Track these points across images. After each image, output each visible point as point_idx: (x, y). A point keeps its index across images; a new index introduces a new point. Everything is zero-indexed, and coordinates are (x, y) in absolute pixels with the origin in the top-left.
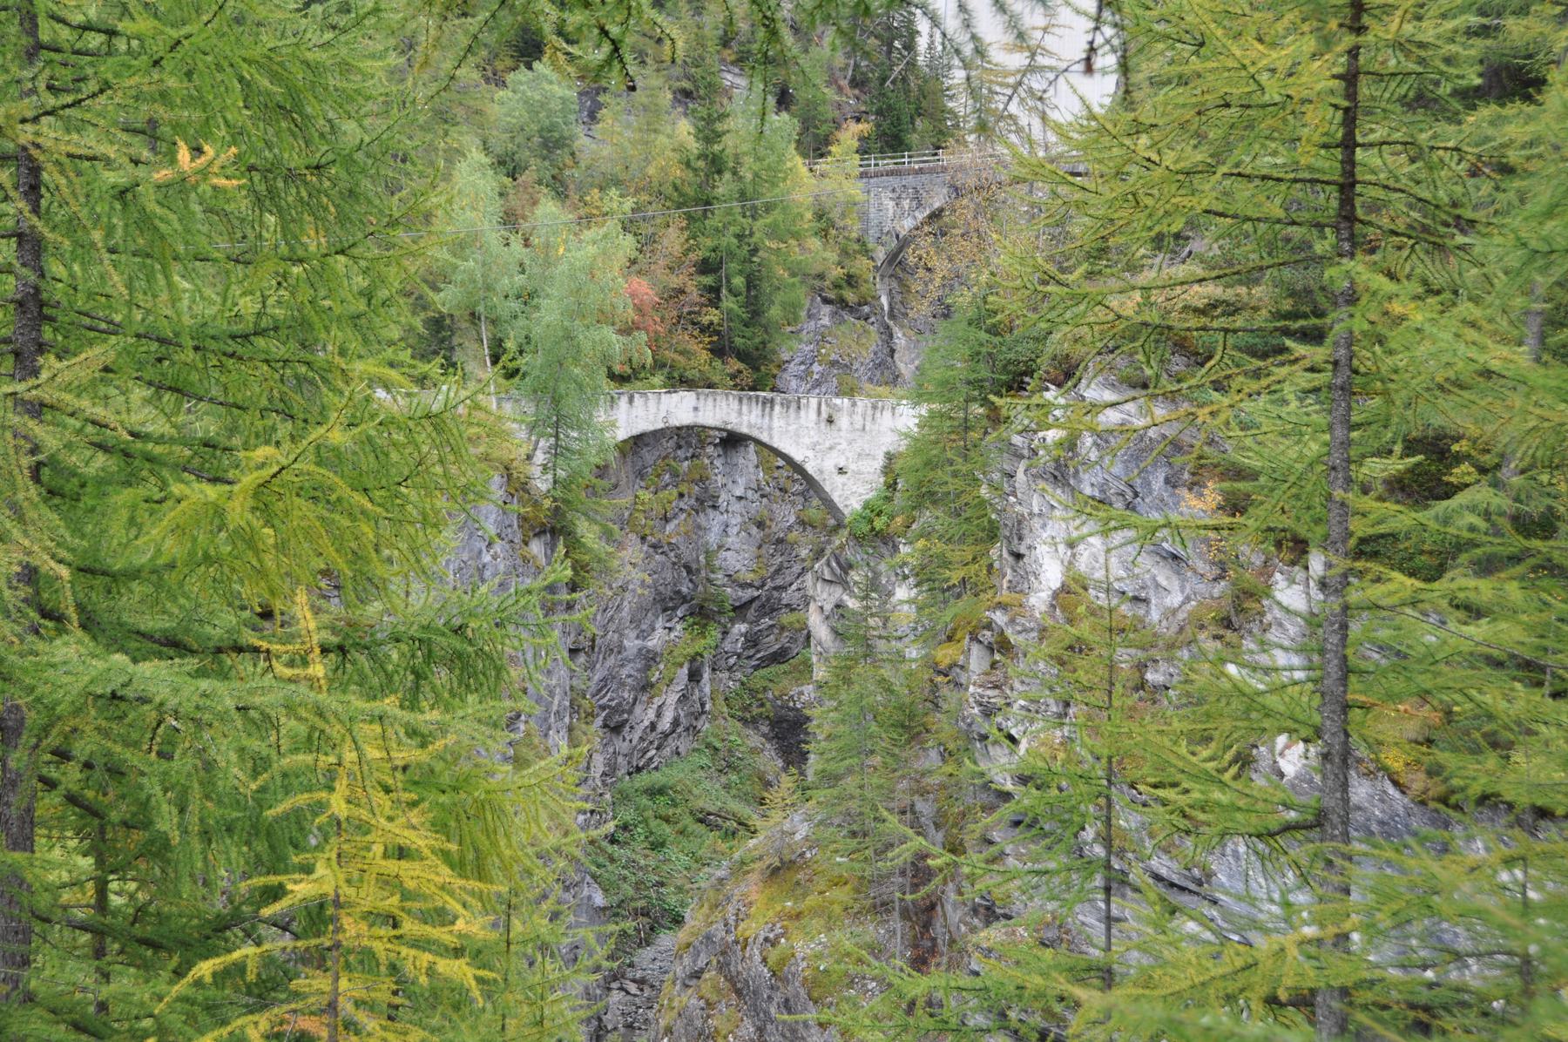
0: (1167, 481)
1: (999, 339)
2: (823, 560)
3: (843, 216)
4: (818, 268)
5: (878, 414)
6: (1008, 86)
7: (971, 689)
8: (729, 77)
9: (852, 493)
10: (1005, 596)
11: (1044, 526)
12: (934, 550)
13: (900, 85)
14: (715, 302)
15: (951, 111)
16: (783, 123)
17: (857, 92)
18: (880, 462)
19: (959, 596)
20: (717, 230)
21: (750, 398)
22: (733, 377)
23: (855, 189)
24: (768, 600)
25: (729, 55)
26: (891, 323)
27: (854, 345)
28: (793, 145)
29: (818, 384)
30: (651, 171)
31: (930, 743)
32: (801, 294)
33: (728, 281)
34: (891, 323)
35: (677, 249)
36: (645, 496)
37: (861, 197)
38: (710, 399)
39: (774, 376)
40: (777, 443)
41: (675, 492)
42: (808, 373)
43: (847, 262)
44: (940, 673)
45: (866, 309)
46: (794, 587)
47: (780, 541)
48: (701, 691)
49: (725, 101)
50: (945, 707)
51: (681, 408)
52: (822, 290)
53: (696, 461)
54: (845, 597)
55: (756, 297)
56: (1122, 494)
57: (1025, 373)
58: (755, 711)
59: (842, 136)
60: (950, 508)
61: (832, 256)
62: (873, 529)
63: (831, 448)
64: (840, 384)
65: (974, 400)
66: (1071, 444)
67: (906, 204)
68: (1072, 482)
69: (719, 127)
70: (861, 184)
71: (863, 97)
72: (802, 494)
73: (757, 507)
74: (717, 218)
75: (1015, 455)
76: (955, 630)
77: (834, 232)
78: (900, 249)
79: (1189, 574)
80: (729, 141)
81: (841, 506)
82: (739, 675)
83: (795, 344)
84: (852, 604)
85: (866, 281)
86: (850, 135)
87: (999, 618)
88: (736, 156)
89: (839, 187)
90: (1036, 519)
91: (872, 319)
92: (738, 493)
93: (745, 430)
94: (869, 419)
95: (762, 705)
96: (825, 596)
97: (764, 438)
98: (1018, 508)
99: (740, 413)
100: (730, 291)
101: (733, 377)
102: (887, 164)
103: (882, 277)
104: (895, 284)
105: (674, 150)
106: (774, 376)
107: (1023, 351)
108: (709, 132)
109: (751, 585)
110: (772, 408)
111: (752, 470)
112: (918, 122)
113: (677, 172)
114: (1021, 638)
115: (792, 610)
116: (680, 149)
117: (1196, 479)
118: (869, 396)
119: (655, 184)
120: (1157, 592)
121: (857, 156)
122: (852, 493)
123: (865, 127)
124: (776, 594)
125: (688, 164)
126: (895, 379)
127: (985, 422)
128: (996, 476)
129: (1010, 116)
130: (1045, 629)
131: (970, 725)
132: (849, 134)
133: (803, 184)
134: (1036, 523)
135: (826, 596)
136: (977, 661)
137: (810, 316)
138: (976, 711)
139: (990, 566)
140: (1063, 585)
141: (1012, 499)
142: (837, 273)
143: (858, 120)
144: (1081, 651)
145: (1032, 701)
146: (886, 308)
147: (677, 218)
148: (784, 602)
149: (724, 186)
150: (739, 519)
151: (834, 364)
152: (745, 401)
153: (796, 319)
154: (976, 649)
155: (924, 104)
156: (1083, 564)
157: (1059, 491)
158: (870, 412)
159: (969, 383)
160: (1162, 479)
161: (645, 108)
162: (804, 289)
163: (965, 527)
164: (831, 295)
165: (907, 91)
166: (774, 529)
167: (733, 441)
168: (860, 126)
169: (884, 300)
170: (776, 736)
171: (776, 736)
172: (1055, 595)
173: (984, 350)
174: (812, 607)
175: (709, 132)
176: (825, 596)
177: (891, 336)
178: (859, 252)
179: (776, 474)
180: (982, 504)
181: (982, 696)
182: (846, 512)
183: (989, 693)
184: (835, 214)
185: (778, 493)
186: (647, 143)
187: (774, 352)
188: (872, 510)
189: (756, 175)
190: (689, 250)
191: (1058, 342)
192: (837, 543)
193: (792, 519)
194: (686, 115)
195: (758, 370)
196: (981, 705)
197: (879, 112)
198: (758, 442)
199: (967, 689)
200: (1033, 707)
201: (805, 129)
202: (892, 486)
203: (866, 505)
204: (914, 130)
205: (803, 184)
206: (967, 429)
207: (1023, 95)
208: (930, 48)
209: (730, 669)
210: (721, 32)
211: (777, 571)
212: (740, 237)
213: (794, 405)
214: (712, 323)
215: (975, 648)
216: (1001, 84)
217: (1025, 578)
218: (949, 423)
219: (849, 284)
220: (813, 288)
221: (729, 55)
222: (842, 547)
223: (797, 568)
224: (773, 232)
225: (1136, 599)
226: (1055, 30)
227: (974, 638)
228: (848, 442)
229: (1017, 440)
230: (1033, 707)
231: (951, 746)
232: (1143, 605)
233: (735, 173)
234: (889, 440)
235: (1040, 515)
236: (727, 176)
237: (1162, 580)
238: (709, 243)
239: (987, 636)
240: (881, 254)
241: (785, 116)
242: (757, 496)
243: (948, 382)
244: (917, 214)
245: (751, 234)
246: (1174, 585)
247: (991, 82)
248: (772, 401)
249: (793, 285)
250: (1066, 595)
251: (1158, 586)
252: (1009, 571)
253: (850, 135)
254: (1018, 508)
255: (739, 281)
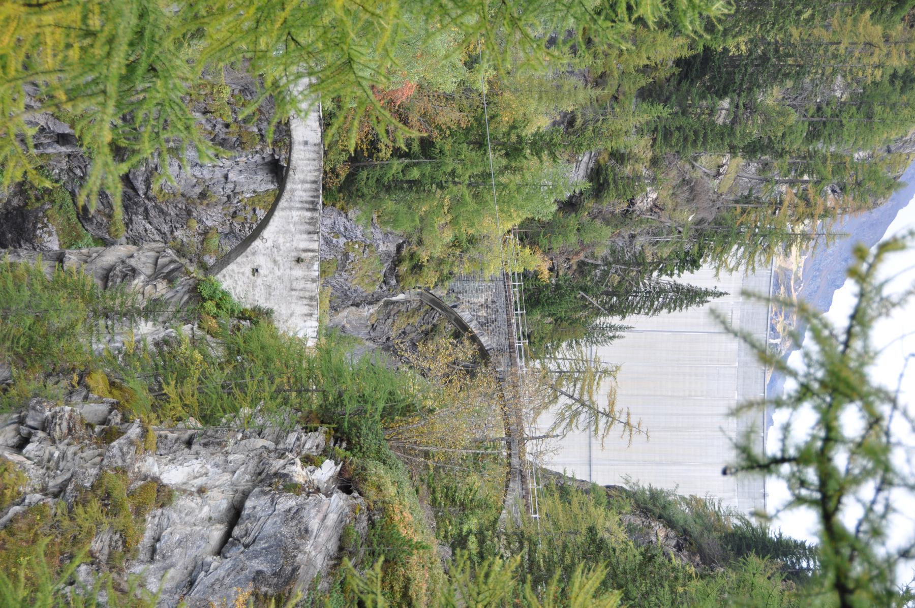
0: (259, 573)
1: (377, 417)
2: (175, 257)
3: (472, 260)
4: (427, 241)
5: (305, 302)
6: (581, 394)
7: (68, 408)
8: (586, 159)
9: (236, 281)
10: (153, 436)
11: (217, 465)
12: (193, 368)
13: (581, 303)
14: (397, 153)
15: (558, 345)
16: (549, 210)
17: (575, 267)
18: (264, 304)
19: (151, 390)
20: (458, 154)
21: (317, 190)
22: (333, 170)
23: (493, 270)
24: (136, 203)
25: (604, 158)
26: (381, 303)
27: (362, 272)
28: (530, 216)
29: (328, 242)
30: (507, 95)
31: (14, 370)
32: (407, 227)
33: (415, 165)
34: (381, 303)
35: (441, 120)
36: (226, 95)
37: (487, 274)
38: (315, 156)
39: (334, 205)
40: (278, 214)
41: (230, 120)
42: (337, 234)
43: (433, 264)
44: (81, 377)
45: (393, 282)
46: (148, 226)
47: (189, 213)
48: (49, 145)
49: (566, 157)
50: (50, 383)
51: (306, 131)
52: (409, 244)
53: (258, 138)
54: (142, 277)
55: (402, 188)
56: (247, 534)
57: (349, 443)
58: (32, 194)
59: (539, 256)
60: (228, 376)
61: (438, 252)
62: (204, 300)
63: (275, 262)
64: (329, 262)
65: (326, 399)
66: (293, 488)
67: (483, 313)
68: (257, 489)
69: (545, 154)
70: (498, 274)
71: (570, 272)
72: (232, 231)
73: (219, 192)
74: (468, 154)
75: (278, 436)
76: (120, 388)
77: (458, 253)
78: (444, 309)
79: (177, 597)
80: (534, 162)
81: (224, 271)
82: (65, 178)
83: (363, 221)
84: (138, 282)
85: (417, 281)
86: (539, 263)
87: (134, 431)
88: (521, 169)
89: (495, 262)
90: (223, 458)
91: (384, 288)
92: (231, 176)
93: (289, 186)
94: (302, 294)
95: (38, 199)
96: (143, 259)
97: (283, 203)
98: (232, 441)
99: (304, 182)
100: (407, 166)
101: (333, 170)
102: (515, 295)
103: (421, 294)
104: (415, 305)
105: (525, 114)
106: (334, 205)
107: (369, 441)
108: (542, 145)
109: (148, 188)
110: (308, 210)
111: (252, 187)
112: (550, 319)
113: (506, 118)
114: (115, 451)
115: (127, 225)
116: (526, 120)
117: (261, 598)
118: (321, 293)
119: (496, 99)
120: (159, 569)
121: (522, 271)
122: (236, 281)
123: (545, 275)
124: (141, 210)
125: (513, 127)
126: (335, 309)
127: (306, 408)
128: (259, 421)
129: (556, 398)
130: (124, 472)
131: (34, 408)
132: (540, 262)
133: (497, 225)
134: (219, 458)
135: (143, 260)
136: (93, 410)
137: (386, 235)
138: (48, 413)
139: (179, 419)
140: (164, 486)
141: (240, 436)
142: (424, 256)
143: (551, 270)
144: (106, 505)
145: (58, 463)
146: (394, 299)
147: (466, 120)
148: (134, 218)
149: (494, 159)
150: (207, 177)
151: (346, 255)
152: (314, 186)
153: (385, 223)
154: (103, 408)
155: (565, 324)
156: (184, 502)
157: (248, 477)
158: (307, 294)
159: (340, 395)
160: (260, 568)
161: (559, 87)
162: (410, 230)
163: (215, 397)
164: (405, 252)
165: (575, 310)
166: (200, 208)
167: (278, 171)
168: (546, 272)
169: (401, 297)
170: (8, 212)
171: (8, 212)
172: (156, 480)
173: (369, 406)
174: (132, 248)
175: (542, 145)
176: (143, 259)
177: (370, 303)
178: (441, 275)
179: (249, 208)
180: (236, 410)
181: (61, 418)
182: (219, 276)
183: (65, 424)
184: (473, 253)
185: (232, 210)
186: (530, 91)
187: (355, 204)
188: (221, 300)
189: (505, 186)
190: (441, 130)
191: (376, 470)
192: (191, 269)
193: (209, 223)
194: (554, 124)
195: (340, 191)
196: (53, 417)
197: (558, 287)
198: (278, 199)
199: (67, 403)
200: (52, 464)
201: (543, 225)
202: (243, 316)
203: (225, 294)
204: (544, 317)
205: (497, 225)
206: (299, 392)
207: (574, 408)
208: (611, 327)
209: (70, 170)
210: (622, 151)
211: (162, 211)
212: (453, 173)
213: (311, 228)
214: (379, 151)
215: (104, 408)
216: (582, 389)
217: (170, 451)
218: (304, 375)
219: (414, 267)
220: (410, 236)
221: (604, 158)
222: (188, 273)
223: (165, 228)
224: (458, 202)
225: (153, 551)
226: (627, 433)
227: (114, 407)
228: (280, 277)
229: (292, 438)
230: (52, 464)
231: (13, 392)
232: (147, 557)
233: (506, 168)
234: (283, 312)
235: (226, 461)
236: (504, 162)
237: (171, 572)
238: (447, 147)
239: (116, 419)
240: (440, 292)
241: (555, 208)
242: (229, 192)
243: (340, 376)
244: (474, 322)
245: (455, 183)
246: (168, 585)
247: (584, 380)
248: (314, 209)
249: (413, 221)
250: (163, 495)
251: (166, 569)
252: (175, 435)
253: (539, 263)
254: (232, 441)
255: (415, 174)
